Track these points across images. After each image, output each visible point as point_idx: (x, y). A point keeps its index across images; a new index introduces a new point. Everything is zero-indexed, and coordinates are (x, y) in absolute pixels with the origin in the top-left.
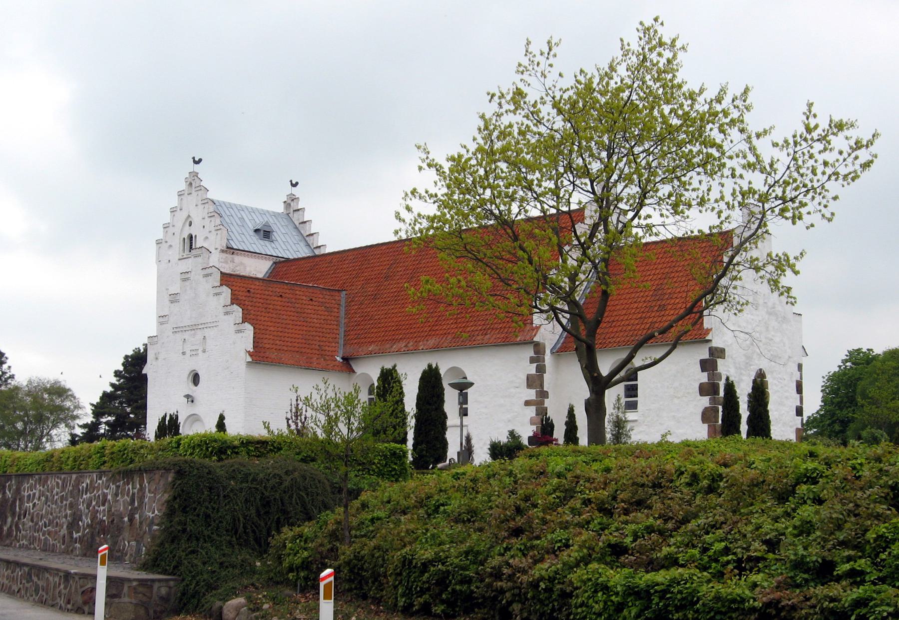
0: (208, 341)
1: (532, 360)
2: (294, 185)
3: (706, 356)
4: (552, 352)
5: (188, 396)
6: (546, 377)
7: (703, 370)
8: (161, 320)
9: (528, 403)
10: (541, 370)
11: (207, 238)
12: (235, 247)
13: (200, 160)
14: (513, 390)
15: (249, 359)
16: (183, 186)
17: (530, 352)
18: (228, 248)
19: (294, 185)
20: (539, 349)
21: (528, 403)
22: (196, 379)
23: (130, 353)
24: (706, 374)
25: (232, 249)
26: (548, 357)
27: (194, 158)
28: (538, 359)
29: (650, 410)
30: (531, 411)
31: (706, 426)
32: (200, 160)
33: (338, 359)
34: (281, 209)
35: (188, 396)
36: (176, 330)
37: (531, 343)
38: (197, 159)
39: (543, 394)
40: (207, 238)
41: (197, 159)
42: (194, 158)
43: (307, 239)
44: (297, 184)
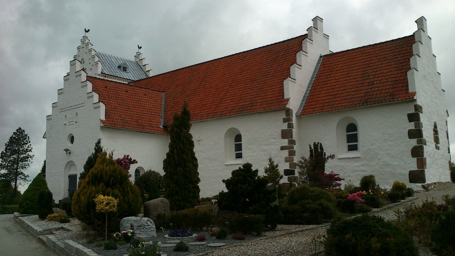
0: (78, 115)
1: (285, 121)
2: (140, 48)
3: (412, 111)
4: (297, 116)
5: (66, 150)
6: (294, 131)
7: (410, 121)
8: (54, 105)
9: (283, 148)
10: (290, 126)
11: (91, 69)
12: (106, 73)
13: (89, 30)
14: (272, 140)
15: (102, 125)
16: (80, 44)
17: (283, 115)
18: (102, 73)
19: (140, 48)
20: (288, 112)
21: (283, 148)
22: (72, 139)
23: (229, 176)
24: (413, 123)
25: (105, 74)
26: (294, 118)
27: (85, 29)
28: (287, 120)
29: (370, 149)
30: (286, 153)
31: (415, 159)
32: (89, 30)
33: (161, 127)
34: (133, 59)
35: (66, 150)
36: (62, 110)
37: (283, 109)
38: (87, 30)
39: (292, 142)
40: (91, 69)
41: (87, 30)
42: (85, 29)
43: (147, 73)
44: (141, 47)
